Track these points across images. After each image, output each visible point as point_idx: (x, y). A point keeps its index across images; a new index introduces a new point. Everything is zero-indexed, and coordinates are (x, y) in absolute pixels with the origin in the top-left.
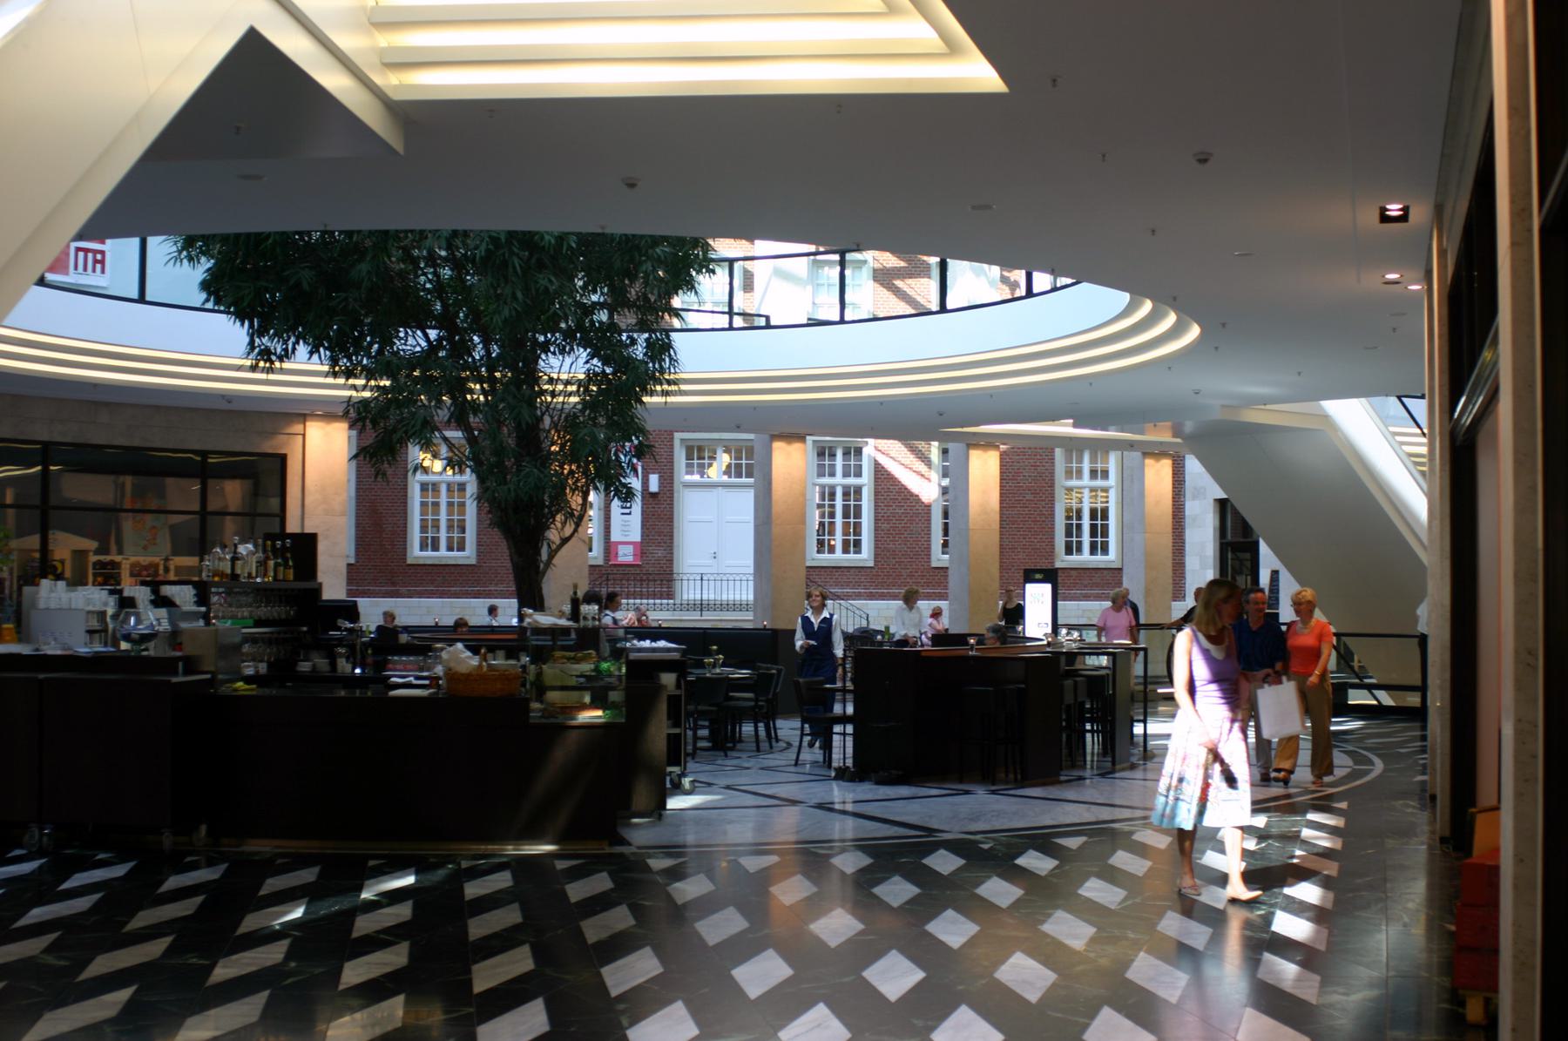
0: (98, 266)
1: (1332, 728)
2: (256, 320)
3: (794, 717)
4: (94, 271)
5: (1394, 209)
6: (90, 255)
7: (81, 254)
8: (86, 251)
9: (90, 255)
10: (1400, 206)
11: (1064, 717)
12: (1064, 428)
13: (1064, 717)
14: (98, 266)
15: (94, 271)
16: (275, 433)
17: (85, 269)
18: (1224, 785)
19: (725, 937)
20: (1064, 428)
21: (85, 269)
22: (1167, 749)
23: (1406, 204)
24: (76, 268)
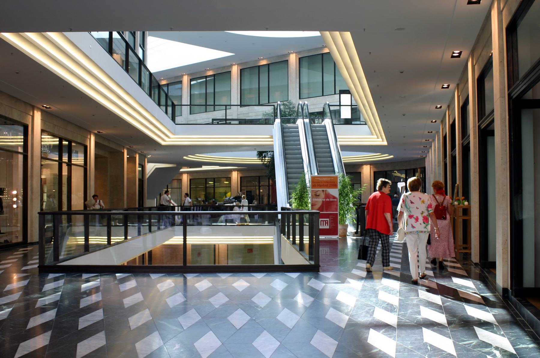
0: (327, 224)
1: (272, 237)
2: (181, 170)
3: (64, 145)
4: (325, 225)
5: (445, 86)
6: (324, 222)
7: (322, 222)
8: (323, 221)
9: (324, 222)
10: (447, 85)
11: (286, 224)
12: (250, 224)
13: (286, 224)
14: (327, 224)
15: (325, 225)
16: (259, 63)
17: (323, 225)
18: (284, 206)
19: (495, 158)
20: (250, 224)
21: (323, 225)
22: (273, 145)
23: (449, 84)
24: (321, 225)
